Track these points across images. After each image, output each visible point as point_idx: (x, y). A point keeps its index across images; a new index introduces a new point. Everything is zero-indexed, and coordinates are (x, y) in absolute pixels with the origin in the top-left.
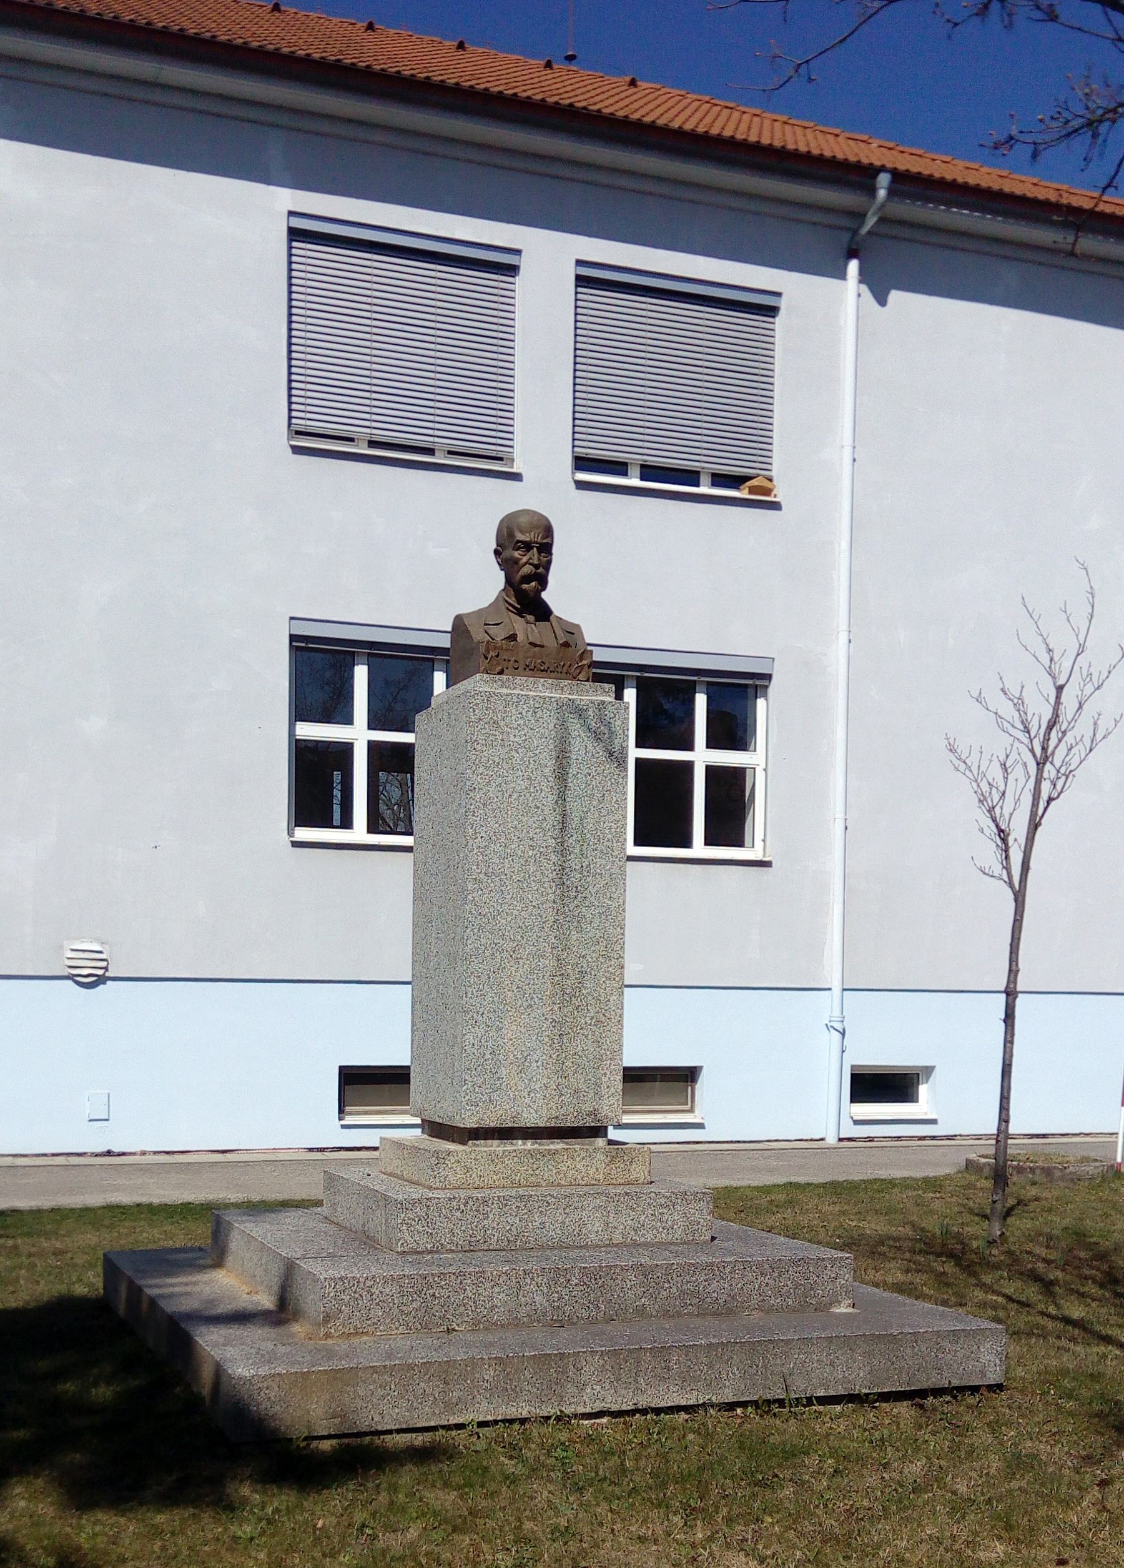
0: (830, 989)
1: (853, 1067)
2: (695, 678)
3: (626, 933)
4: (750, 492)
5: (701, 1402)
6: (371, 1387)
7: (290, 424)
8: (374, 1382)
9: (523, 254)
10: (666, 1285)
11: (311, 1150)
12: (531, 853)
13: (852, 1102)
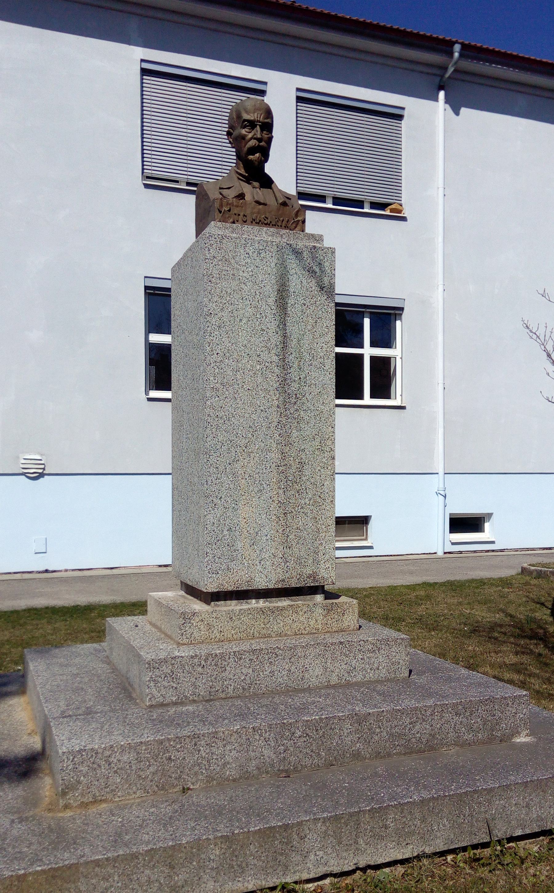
0: (438, 473)
1: (450, 514)
2: (364, 310)
3: (336, 432)
4: (391, 212)
5: (415, 854)
6: (94, 881)
7: (143, 173)
8: (97, 875)
9: (268, 84)
10: (378, 730)
11: (160, 566)
12: (258, 367)
13: (450, 533)
